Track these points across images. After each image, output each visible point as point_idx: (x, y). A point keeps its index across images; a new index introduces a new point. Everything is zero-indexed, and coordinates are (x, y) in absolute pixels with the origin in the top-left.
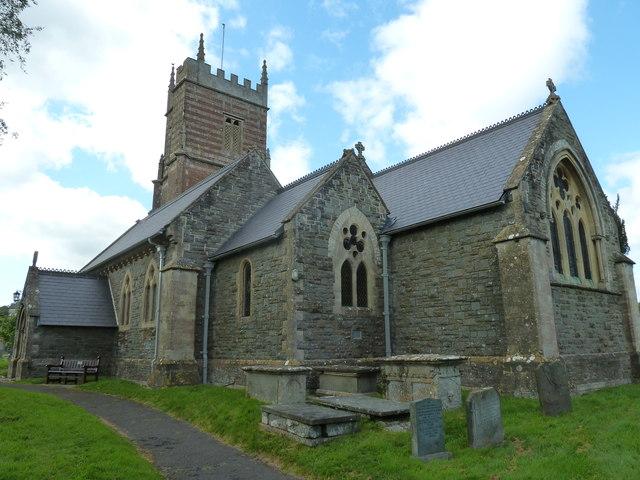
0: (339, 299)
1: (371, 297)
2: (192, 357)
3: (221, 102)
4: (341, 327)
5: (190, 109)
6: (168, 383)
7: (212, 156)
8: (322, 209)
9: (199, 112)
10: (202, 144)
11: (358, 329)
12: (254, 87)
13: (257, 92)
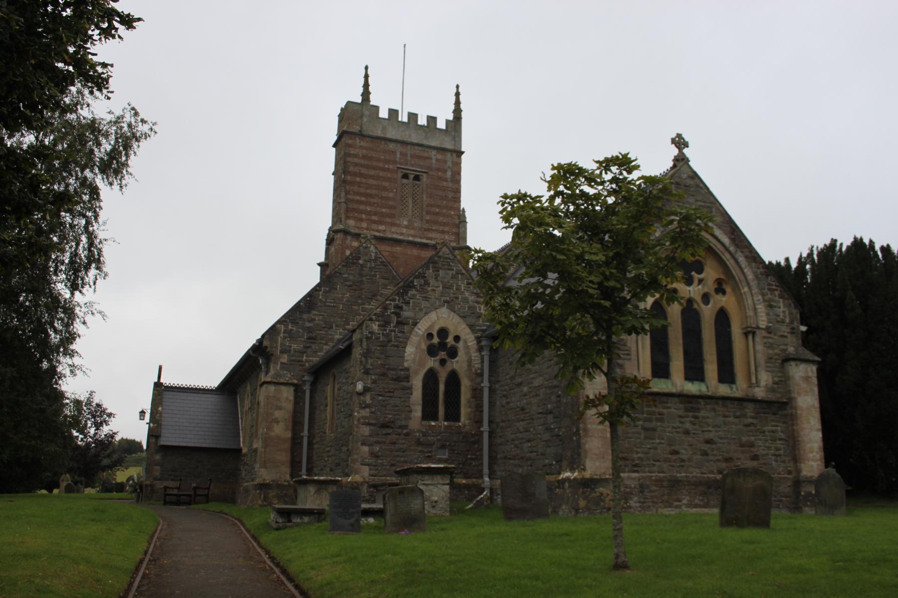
0: (418, 412)
1: (465, 411)
2: (288, 477)
3: (394, 152)
4: (419, 443)
5: (351, 169)
6: (260, 502)
7: (382, 227)
8: (398, 315)
9: (364, 171)
10: (369, 213)
11: (443, 447)
12: (441, 125)
13: (446, 131)
